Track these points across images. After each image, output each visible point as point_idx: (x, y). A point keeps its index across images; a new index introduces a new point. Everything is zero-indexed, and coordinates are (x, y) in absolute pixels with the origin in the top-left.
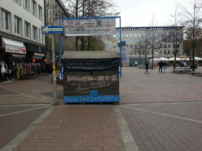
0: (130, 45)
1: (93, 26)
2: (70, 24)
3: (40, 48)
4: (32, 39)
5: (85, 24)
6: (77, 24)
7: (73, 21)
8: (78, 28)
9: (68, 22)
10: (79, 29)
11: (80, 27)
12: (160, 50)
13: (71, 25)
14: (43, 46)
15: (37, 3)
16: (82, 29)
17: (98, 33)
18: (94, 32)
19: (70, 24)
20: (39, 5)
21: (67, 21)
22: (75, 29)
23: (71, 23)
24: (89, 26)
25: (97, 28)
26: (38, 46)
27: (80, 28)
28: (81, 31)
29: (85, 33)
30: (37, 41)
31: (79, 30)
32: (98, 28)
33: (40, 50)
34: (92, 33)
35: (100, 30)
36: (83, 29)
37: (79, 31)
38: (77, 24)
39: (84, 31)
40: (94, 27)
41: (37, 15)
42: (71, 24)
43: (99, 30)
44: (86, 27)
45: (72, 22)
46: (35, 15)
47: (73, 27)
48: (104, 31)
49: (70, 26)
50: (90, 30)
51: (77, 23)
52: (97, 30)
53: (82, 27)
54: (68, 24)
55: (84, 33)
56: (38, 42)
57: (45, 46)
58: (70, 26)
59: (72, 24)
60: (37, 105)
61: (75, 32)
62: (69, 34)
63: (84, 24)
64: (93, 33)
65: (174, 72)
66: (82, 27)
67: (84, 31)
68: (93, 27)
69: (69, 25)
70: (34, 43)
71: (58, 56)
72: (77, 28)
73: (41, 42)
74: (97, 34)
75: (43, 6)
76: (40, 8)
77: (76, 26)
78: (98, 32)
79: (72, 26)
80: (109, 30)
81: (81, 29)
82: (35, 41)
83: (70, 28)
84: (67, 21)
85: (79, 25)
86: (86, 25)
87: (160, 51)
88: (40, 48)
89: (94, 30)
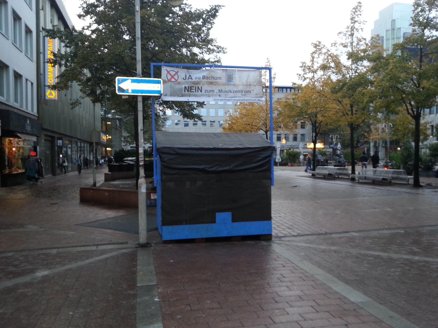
0: (211, 122)
1: (217, 84)
2: (173, 77)
3: (28, 122)
4: (12, 102)
5: (204, 77)
6: (187, 78)
7: (178, 72)
8: (188, 85)
9: (168, 72)
10: (191, 87)
11: (193, 83)
12: (278, 133)
13: (175, 79)
14: (33, 117)
15: (23, 20)
16: (196, 87)
17: (228, 96)
18: (219, 95)
19: (173, 77)
20: (26, 27)
21: (167, 70)
22: (183, 86)
23: (175, 75)
24: (211, 83)
25: (226, 86)
26: (25, 118)
27: (192, 85)
28: (194, 90)
29: (203, 95)
30: (21, 106)
31: (191, 89)
32: (227, 88)
33: (29, 128)
34: (215, 96)
35: (232, 92)
36: (198, 88)
37: (191, 91)
38: (187, 78)
39: (201, 91)
40: (221, 85)
41: (21, 47)
42: (175, 77)
43: (231, 92)
44: (204, 85)
45: (177, 73)
46: (18, 46)
47: (179, 83)
48: (240, 94)
49: (173, 80)
50: (213, 91)
51: (186, 75)
52: (226, 92)
53: (196, 84)
54: (169, 77)
55: (200, 97)
56: (24, 109)
57: (36, 118)
58: (173, 80)
59: (176, 77)
60: (101, 248)
61: (183, 92)
62: (171, 96)
63: (201, 77)
64: (218, 96)
65: (313, 176)
66: (197, 83)
67: (201, 91)
68: (218, 85)
69: (171, 78)
70: (16, 111)
71: (61, 141)
72: (187, 86)
73: (29, 110)
74: (226, 99)
75: (33, 28)
76: (28, 31)
77: (184, 81)
78: (228, 95)
79: (176, 81)
80: (249, 92)
81: (194, 88)
82: (17, 105)
83: (173, 84)
84: (167, 70)
85: (190, 80)
86: (205, 80)
87: (278, 135)
88: (28, 122)
89: (220, 91)
